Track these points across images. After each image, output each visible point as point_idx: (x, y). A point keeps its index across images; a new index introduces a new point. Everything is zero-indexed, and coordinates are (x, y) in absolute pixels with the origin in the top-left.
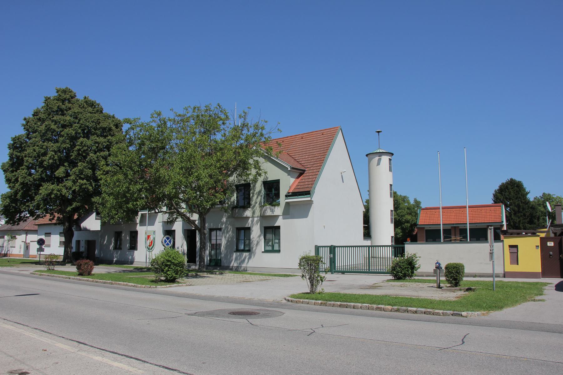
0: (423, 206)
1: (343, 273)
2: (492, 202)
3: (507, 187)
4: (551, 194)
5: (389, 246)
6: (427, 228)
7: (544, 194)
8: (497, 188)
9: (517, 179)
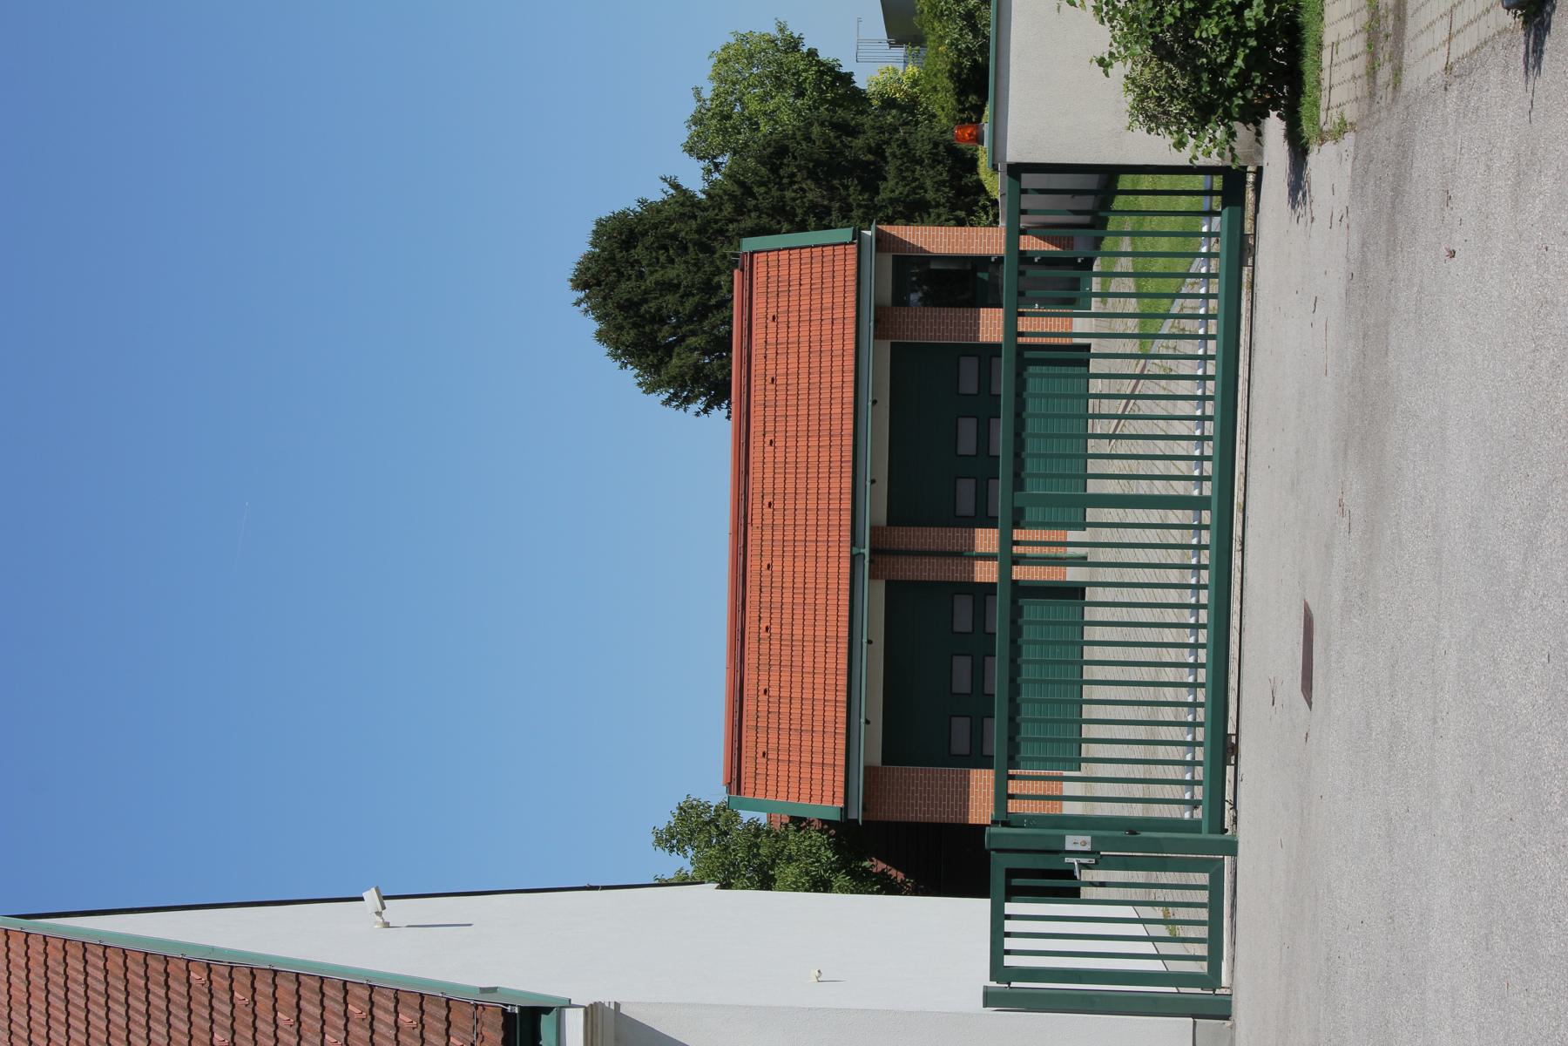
0: (714, 793)
1: (1224, 750)
2: (718, 414)
3: (628, 306)
4: (692, 107)
5: (998, 918)
6: (871, 749)
7: (690, 149)
8: (628, 377)
9: (579, 245)
